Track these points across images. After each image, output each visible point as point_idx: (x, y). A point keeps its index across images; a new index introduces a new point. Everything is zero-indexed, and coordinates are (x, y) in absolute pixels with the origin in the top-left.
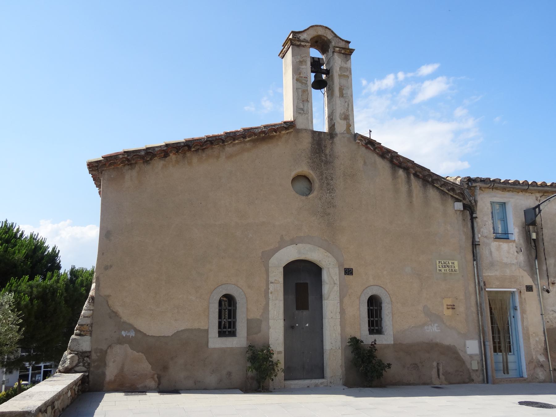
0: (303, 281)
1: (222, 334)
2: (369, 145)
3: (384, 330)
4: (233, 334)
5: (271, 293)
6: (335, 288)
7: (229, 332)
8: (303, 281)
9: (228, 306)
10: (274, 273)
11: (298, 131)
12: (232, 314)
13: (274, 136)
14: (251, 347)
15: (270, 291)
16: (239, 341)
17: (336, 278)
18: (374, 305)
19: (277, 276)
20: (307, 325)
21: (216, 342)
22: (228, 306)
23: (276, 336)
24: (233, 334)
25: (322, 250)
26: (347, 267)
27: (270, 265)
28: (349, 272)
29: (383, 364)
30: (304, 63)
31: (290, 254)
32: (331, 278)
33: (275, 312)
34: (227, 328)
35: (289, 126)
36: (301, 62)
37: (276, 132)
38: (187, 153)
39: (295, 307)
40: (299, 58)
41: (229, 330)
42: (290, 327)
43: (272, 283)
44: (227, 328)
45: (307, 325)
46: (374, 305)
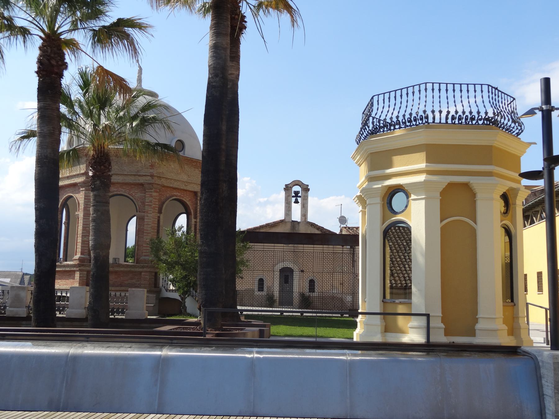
0: (286, 275)
3: (36, 75)
4: (263, 291)
8: (286, 275)
9: (261, 281)
11: (286, 222)
12: (263, 284)
14: (268, 295)
16: (264, 293)
18: (312, 282)
19: (277, 274)
21: (257, 293)
22: (261, 281)
23: (276, 294)
24: (263, 291)
28: (302, 271)
29: (42, 44)
31: (280, 266)
34: (261, 288)
35: (282, 221)
36: (288, 196)
40: (288, 195)
42: (281, 291)
44: (261, 288)
46: (312, 282)
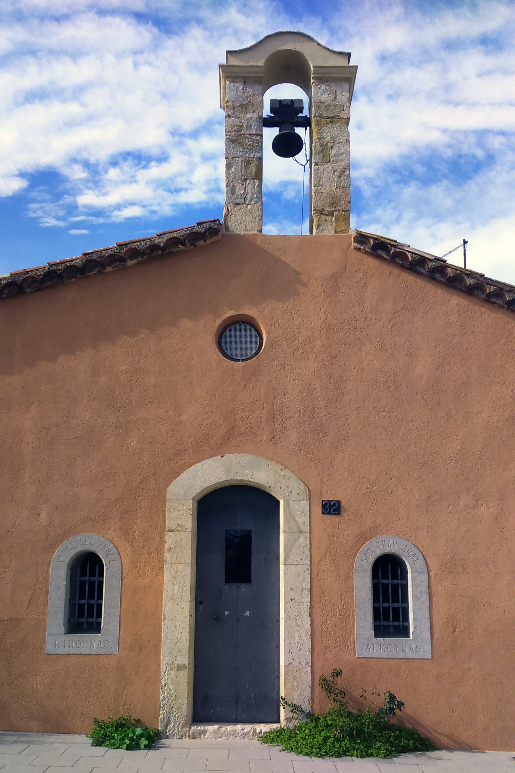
1: (381, 631)
2: (379, 252)
4: (96, 628)
5: (170, 550)
6: (302, 540)
7: (396, 628)
10: (176, 513)
13: (181, 252)
15: (166, 546)
17: (303, 520)
20: (247, 613)
24: (96, 628)
25: (274, 465)
26: (329, 497)
27: (168, 497)
28: (332, 508)
30: (250, 108)
31: (209, 473)
32: (294, 518)
33: (176, 588)
37: (184, 244)
38: (413, 183)
39: (224, 578)
41: (396, 624)
43: (171, 530)
45: (247, 613)
46: (388, 573)
